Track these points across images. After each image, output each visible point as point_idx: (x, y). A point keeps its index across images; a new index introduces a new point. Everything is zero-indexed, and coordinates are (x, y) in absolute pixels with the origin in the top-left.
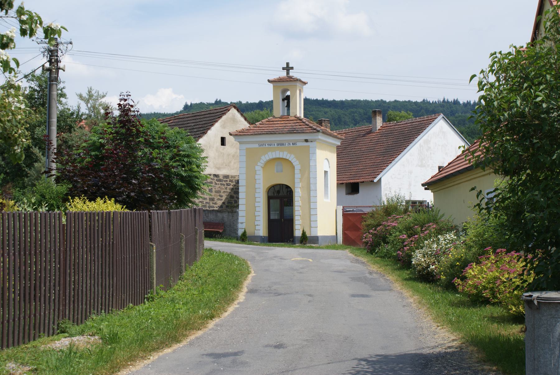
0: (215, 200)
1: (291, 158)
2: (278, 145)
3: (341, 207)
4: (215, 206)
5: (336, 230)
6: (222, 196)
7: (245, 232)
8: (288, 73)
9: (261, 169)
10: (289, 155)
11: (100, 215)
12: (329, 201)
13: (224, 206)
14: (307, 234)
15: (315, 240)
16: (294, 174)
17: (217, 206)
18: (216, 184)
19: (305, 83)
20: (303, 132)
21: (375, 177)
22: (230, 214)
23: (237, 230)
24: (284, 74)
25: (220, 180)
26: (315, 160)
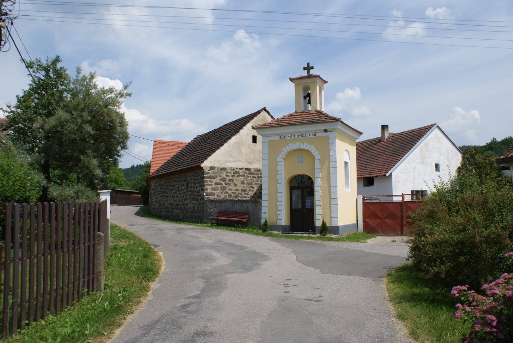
0: (247, 191)
1: (311, 148)
2: (298, 136)
3: (362, 197)
4: (247, 196)
5: (357, 218)
6: (254, 188)
7: (266, 222)
8: (309, 72)
9: (283, 161)
10: (309, 146)
11: (93, 206)
12: (349, 190)
13: (256, 196)
14: (326, 224)
15: (335, 230)
16: (314, 164)
17: (249, 196)
18: (248, 177)
19: (326, 82)
20: (322, 122)
21: (387, 172)
22: (254, 204)
23: (260, 219)
24: (305, 73)
25: (252, 174)
26: (335, 150)
